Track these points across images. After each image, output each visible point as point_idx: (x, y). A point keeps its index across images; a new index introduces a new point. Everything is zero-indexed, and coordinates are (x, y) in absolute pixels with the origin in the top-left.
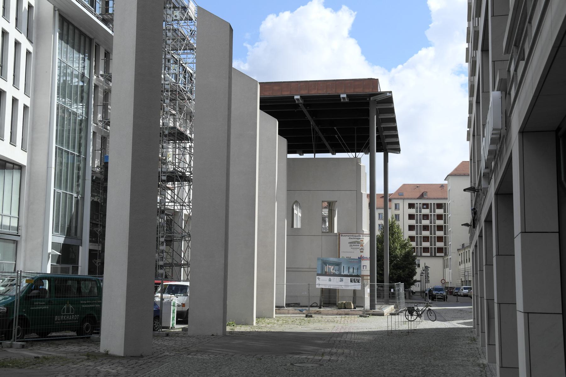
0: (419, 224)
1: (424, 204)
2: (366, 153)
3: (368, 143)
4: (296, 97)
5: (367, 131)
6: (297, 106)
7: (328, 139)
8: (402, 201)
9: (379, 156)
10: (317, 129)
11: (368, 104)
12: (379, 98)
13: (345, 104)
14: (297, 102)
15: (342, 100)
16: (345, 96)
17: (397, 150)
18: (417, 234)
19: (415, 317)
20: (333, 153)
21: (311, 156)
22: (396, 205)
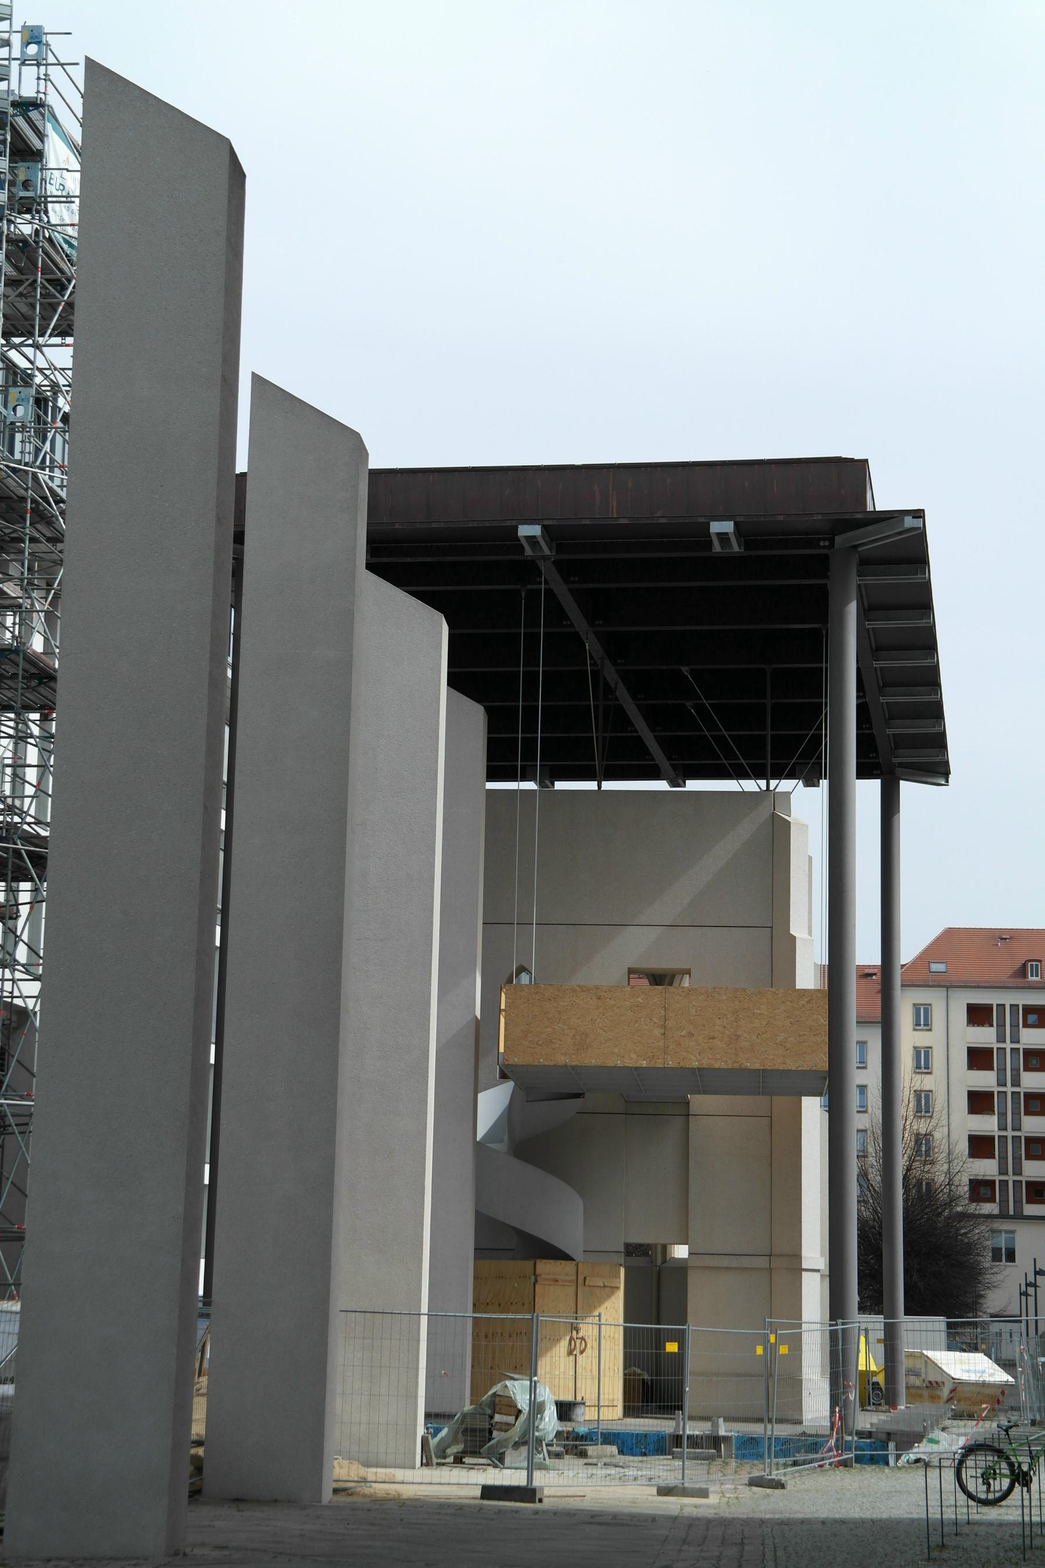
0: (1009, 1089)
1: (1028, 1010)
2: (811, 781)
3: (817, 740)
4: (526, 530)
5: (812, 686)
6: (529, 570)
7: (652, 717)
8: (941, 993)
9: (866, 793)
10: (610, 674)
11: (821, 565)
12: (868, 539)
13: (726, 564)
14: (528, 551)
15: (717, 547)
16: (727, 527)
17: (934, 767)
18: (1002, 1127)
19: (1006, 1483)
20: (677, 778)
21: (591, 785)
22: (917, 1007)
